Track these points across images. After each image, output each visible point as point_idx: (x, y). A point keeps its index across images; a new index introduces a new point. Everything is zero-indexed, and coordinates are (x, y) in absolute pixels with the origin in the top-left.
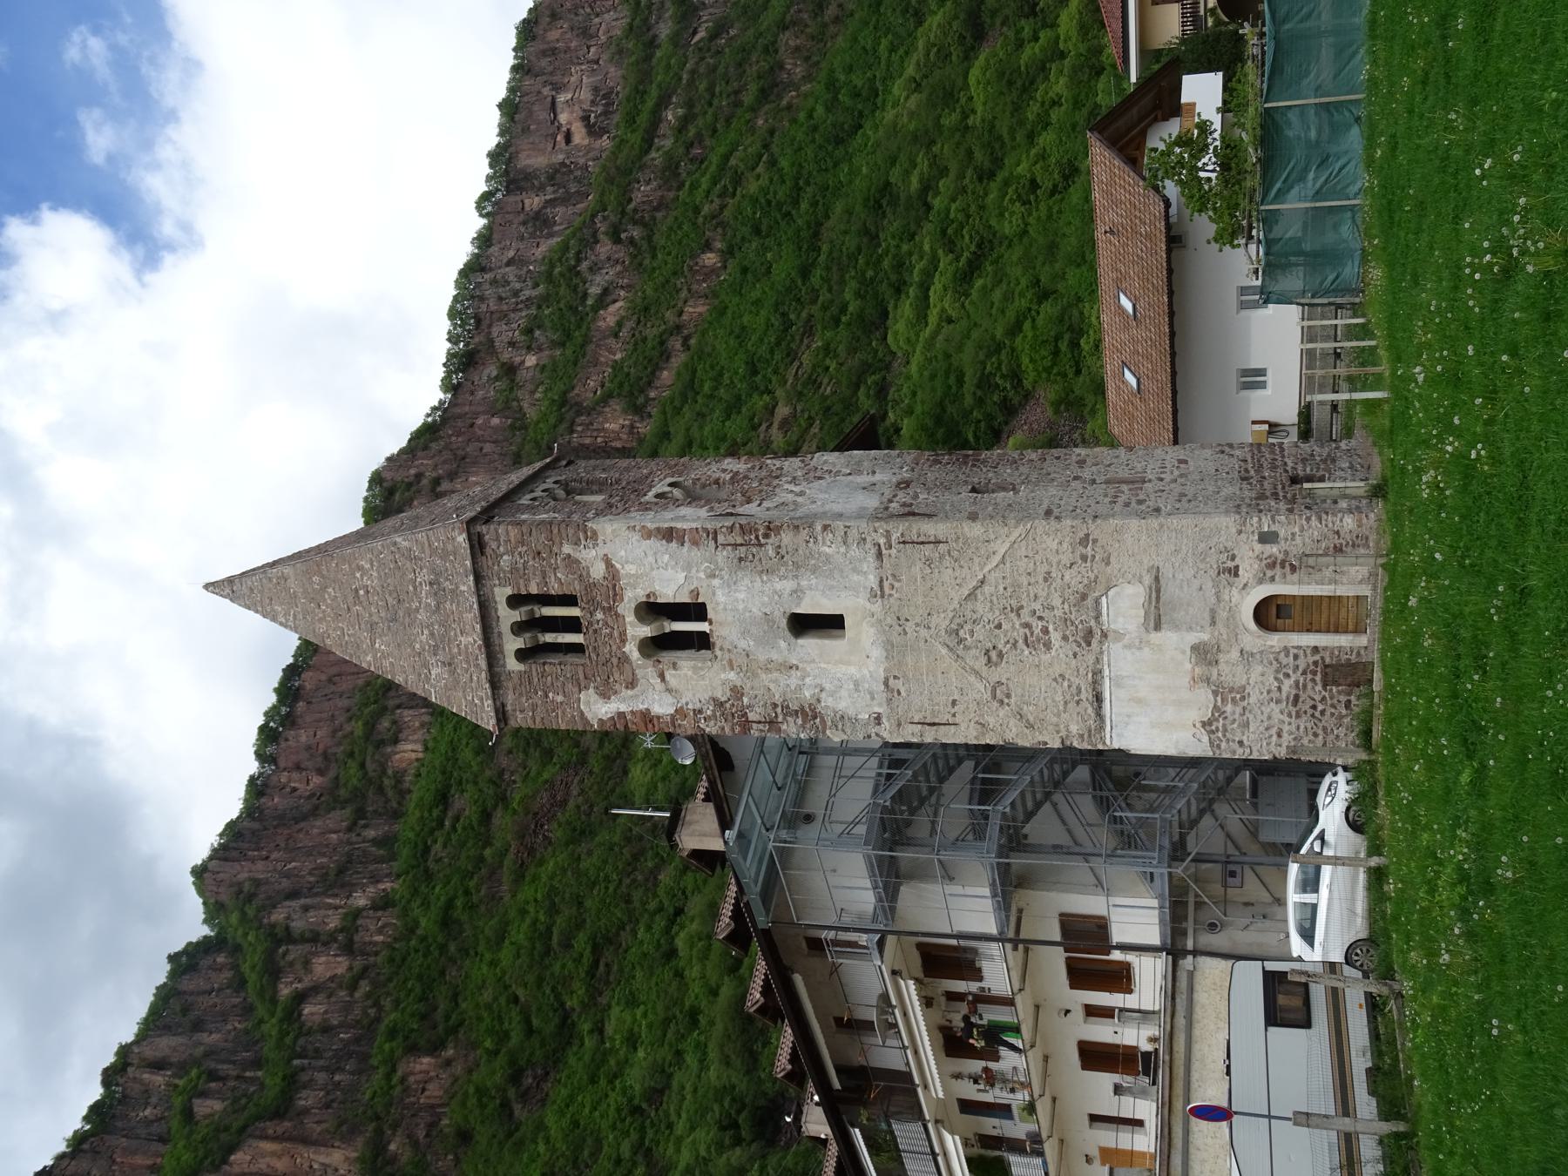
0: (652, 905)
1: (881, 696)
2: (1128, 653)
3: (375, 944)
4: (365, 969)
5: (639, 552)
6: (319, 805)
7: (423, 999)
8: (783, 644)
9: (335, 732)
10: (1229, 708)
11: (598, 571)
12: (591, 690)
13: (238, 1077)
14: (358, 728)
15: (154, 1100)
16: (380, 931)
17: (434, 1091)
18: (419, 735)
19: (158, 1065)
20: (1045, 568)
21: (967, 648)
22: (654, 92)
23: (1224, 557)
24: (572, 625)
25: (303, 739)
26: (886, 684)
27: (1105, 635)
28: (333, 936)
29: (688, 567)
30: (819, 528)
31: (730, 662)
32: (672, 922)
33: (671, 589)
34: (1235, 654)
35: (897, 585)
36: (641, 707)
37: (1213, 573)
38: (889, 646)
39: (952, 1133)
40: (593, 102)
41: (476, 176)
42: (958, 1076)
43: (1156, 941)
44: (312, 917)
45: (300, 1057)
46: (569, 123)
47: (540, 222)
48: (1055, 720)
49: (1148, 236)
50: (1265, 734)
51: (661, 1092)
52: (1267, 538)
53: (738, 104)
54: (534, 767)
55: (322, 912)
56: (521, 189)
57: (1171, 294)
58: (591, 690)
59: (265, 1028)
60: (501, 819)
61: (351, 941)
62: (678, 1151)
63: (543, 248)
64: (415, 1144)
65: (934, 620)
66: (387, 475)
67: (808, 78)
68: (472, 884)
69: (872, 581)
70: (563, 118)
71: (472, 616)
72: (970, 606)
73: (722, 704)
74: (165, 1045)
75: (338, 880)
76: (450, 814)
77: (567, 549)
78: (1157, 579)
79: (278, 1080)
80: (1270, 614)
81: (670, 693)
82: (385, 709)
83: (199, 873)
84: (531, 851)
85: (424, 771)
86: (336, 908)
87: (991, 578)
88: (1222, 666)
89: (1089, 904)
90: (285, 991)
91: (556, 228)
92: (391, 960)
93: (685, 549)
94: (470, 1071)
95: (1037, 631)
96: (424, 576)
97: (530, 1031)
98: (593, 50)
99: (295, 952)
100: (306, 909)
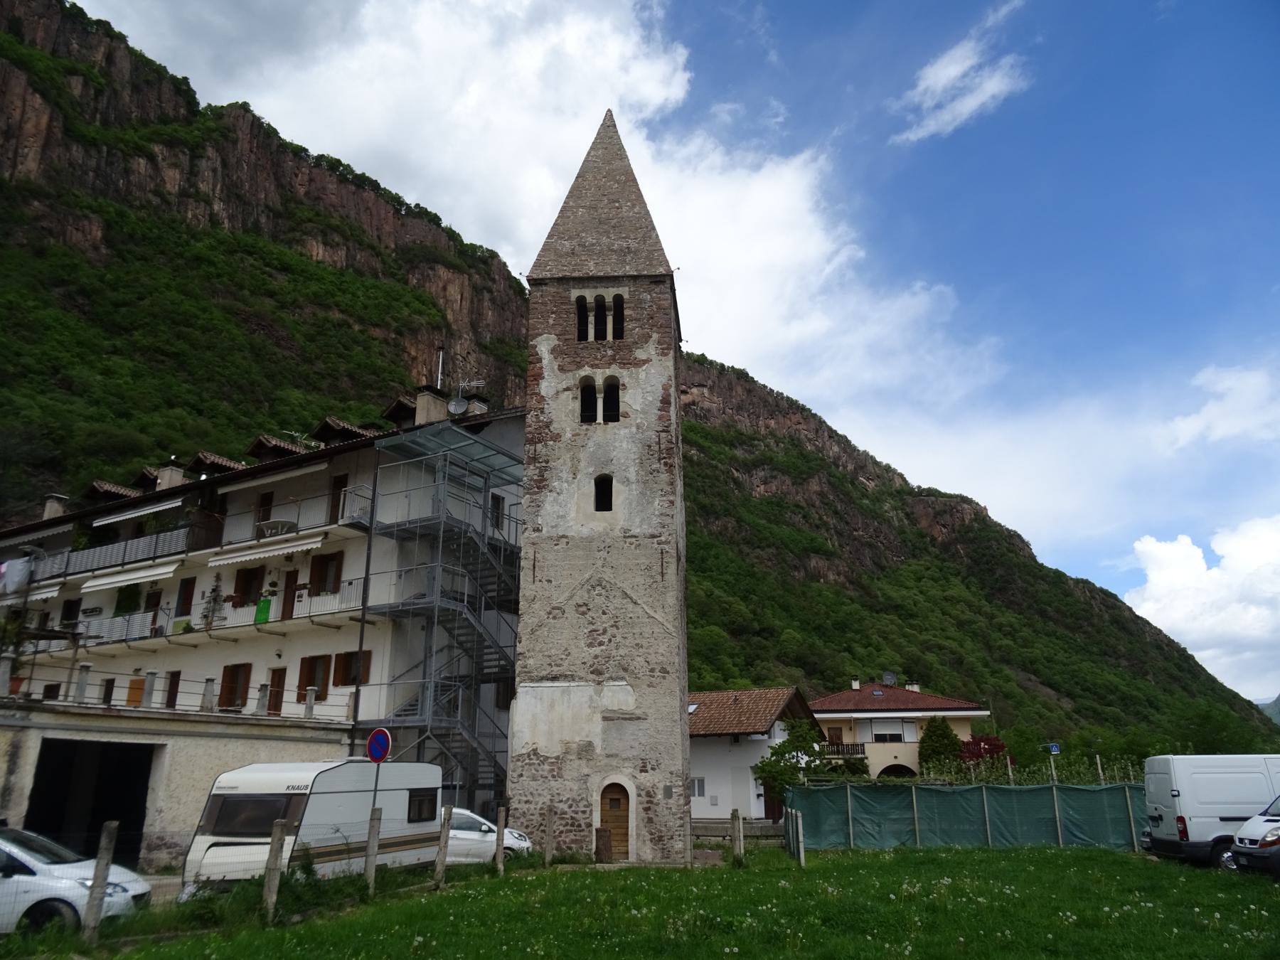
0: (205, 395)
1: (554, 533)
2: (586, 699)
3: (186, 212)
4: (168, 203)
5: (654, 382)
6: (284, 188)
7: (144, 237)
8: (591, 470)
9: (334, 206)
10: (547, 767)
11: (640, 354)
13: (96, 109)
14: (335, 221)
15: (84, 51)
16: (195, 216)
17: (77, 237)
18: (328, 258)
19: (109, 58)
21: (589, 591)
22: (707, 444)
23: (654, 762)
24: (600, 335)
25: (330, 186)
26: (563, 536)
27: (599, 683)
28: (194, 185)
29: (644, 412)
30: (672, 498)
31: (578, 435)
32: (193, 407)
33: (629, 400)
34: (586, 771)
36: (546, 374)
37: (643, 755)
38: (590, 539)
39: (175, 571)
42: (218, 578)
43: (362, 717)
44: (208, 174)
45: (108, 152)
49: (740, 722)
50: (524, 789)
51: (69, 389)
52: (668, 792)
53: (698, 491)
54: (304, 329)
55: (211, 181)
57: (705, 736)
59: (131, 132)
60: (269, 303)
61: (189, 196)
62: (25, 396)
64: (37, 218)
65: (608, 570)
66: (495, 262)
67: (710, 533)
68: (225, 279)
70: (695, 390)
71: (608, 270)
72: (618, 594)
73: (548, 427)
74: (124, 65)
75: (232, 194)
76: (274, 272)
77: (655, 336)
78: (639, 718)
79: (93, 135)
80: (615, 795)
81: (555, 392)
82: (347, 240)
83: (245, 107)
84: (246, 321)
85: (304, 258)
86: (213, 190)
87: (638, 609)
88: (577, 762)
89: (380, 670)
90: (157, 149)
92: (174, 221)
94: (89, 262)
95: (601, 638)
96: (633, 245)
97: (117, 305)
99: (184, 159)
100: (214, 170)
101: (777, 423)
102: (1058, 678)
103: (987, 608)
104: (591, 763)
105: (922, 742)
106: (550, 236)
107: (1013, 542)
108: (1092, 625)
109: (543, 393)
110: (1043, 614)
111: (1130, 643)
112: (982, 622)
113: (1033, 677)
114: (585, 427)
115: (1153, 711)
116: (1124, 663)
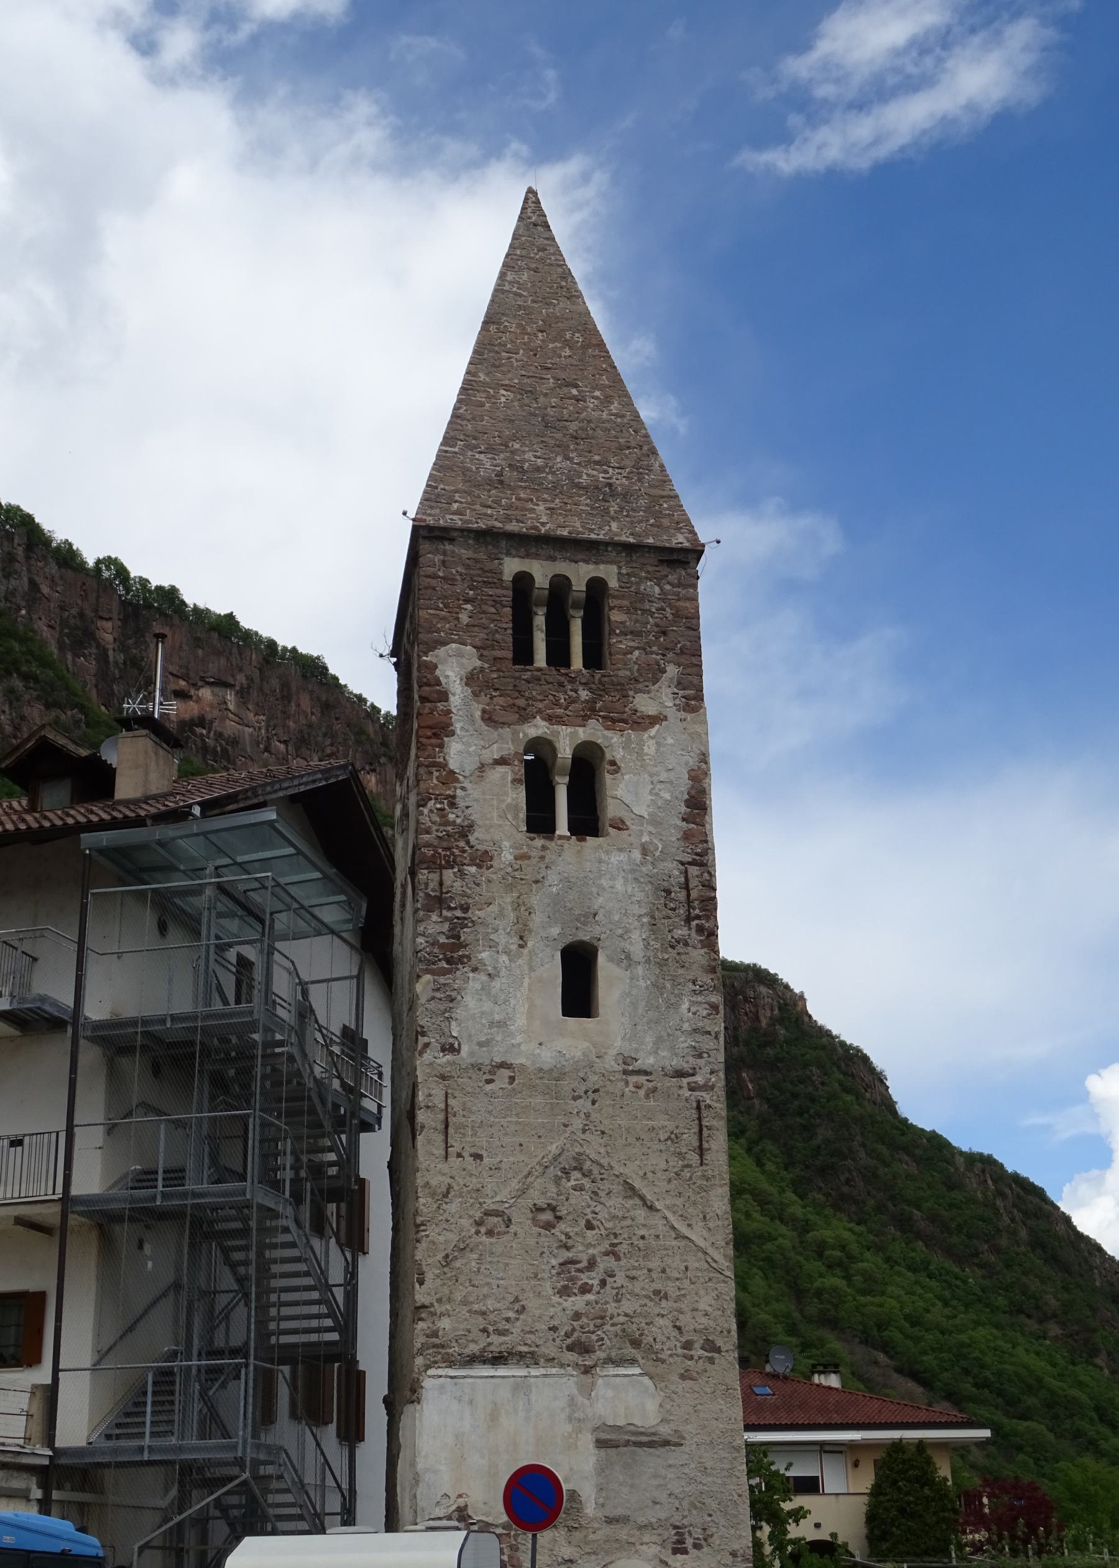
1: (484, 1057)
8: (555, 931)
11: (644, 704)
12: (478, 663)
20: (672, 1292)
21: (557, 1180)
23: (698, 1533)
24: (559, 655)
26: (503, 1065)
27: (587, 1370)
29: (654, 821)
34: (567, 1552)
35: (642, 1093)
36: (458, 726)
37: (677, 1519)
38: (557, 1074)
40: (220, 735)
41: (150, 567)
46: (199, 700)
47: (81, 637)
48: (458, 1296)
56: (125, 621)
58: (478, 663)
63: (46, 633)
65: (595, 1139)
69: (647, 1061)
70: (206, 693)
71: (572, 527)
72: (617, 1188)
77: (672, 671)
78: (666, 1443)
91: (69, 656)
93: (679, 823)
95: (584, 1278)
96: (621, 482)
98: (282, 747)
101: (382, 781)
102: (929, 1360)
103: (797, 1210)
104: (577, 1535)
105: (876, 1492)
106: (447, 440)
107: (853, 1070)
108: (996, 1250)
109: (453, 765)
110: (903, 1223)
111: (1066, 1288)
112: (786, 1237)
113: (881, 1357)
114: (539, 842)
115: (1105, 1430)
116: (1054, 1329)
